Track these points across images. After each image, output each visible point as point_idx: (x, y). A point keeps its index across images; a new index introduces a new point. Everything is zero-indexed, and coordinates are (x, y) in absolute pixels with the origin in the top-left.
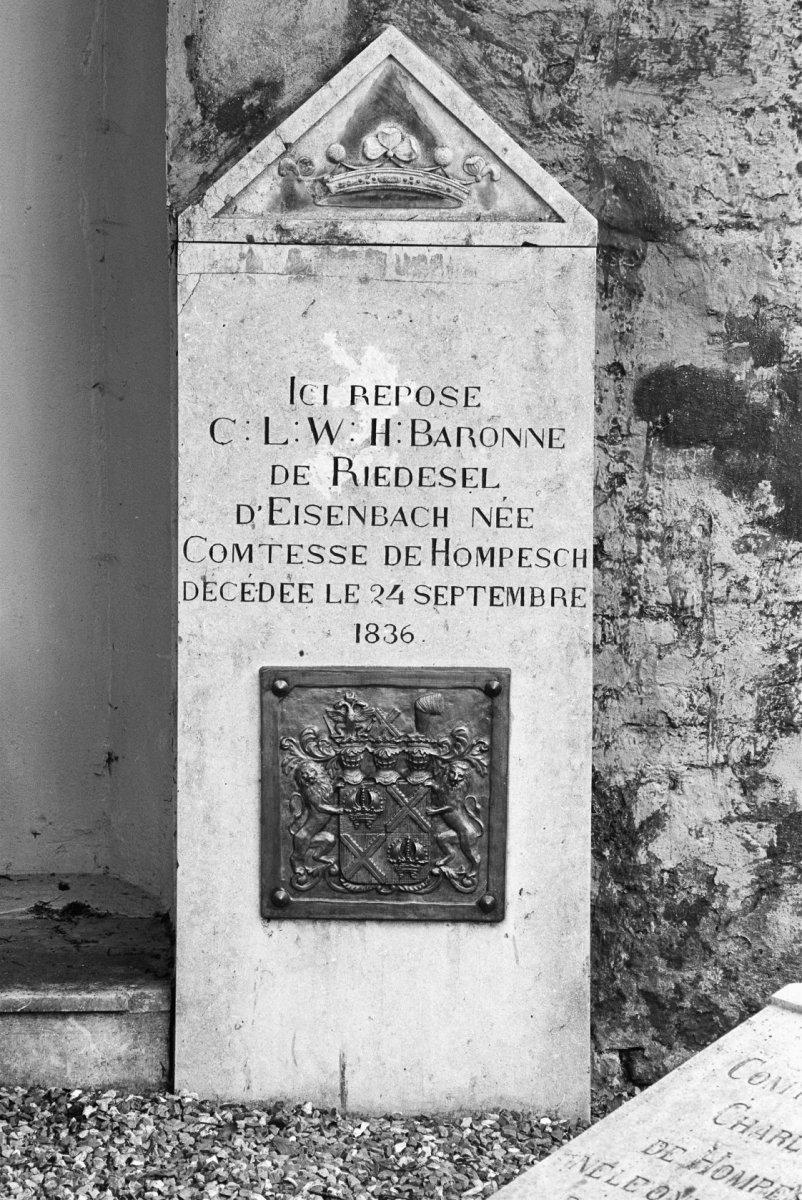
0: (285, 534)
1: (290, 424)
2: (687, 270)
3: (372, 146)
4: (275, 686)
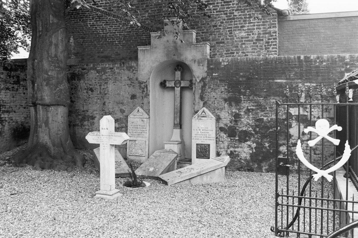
0: (198, 136)
1: (198, 129)
2: (222, 121)
3: (202, 114)
4: (197, 144)
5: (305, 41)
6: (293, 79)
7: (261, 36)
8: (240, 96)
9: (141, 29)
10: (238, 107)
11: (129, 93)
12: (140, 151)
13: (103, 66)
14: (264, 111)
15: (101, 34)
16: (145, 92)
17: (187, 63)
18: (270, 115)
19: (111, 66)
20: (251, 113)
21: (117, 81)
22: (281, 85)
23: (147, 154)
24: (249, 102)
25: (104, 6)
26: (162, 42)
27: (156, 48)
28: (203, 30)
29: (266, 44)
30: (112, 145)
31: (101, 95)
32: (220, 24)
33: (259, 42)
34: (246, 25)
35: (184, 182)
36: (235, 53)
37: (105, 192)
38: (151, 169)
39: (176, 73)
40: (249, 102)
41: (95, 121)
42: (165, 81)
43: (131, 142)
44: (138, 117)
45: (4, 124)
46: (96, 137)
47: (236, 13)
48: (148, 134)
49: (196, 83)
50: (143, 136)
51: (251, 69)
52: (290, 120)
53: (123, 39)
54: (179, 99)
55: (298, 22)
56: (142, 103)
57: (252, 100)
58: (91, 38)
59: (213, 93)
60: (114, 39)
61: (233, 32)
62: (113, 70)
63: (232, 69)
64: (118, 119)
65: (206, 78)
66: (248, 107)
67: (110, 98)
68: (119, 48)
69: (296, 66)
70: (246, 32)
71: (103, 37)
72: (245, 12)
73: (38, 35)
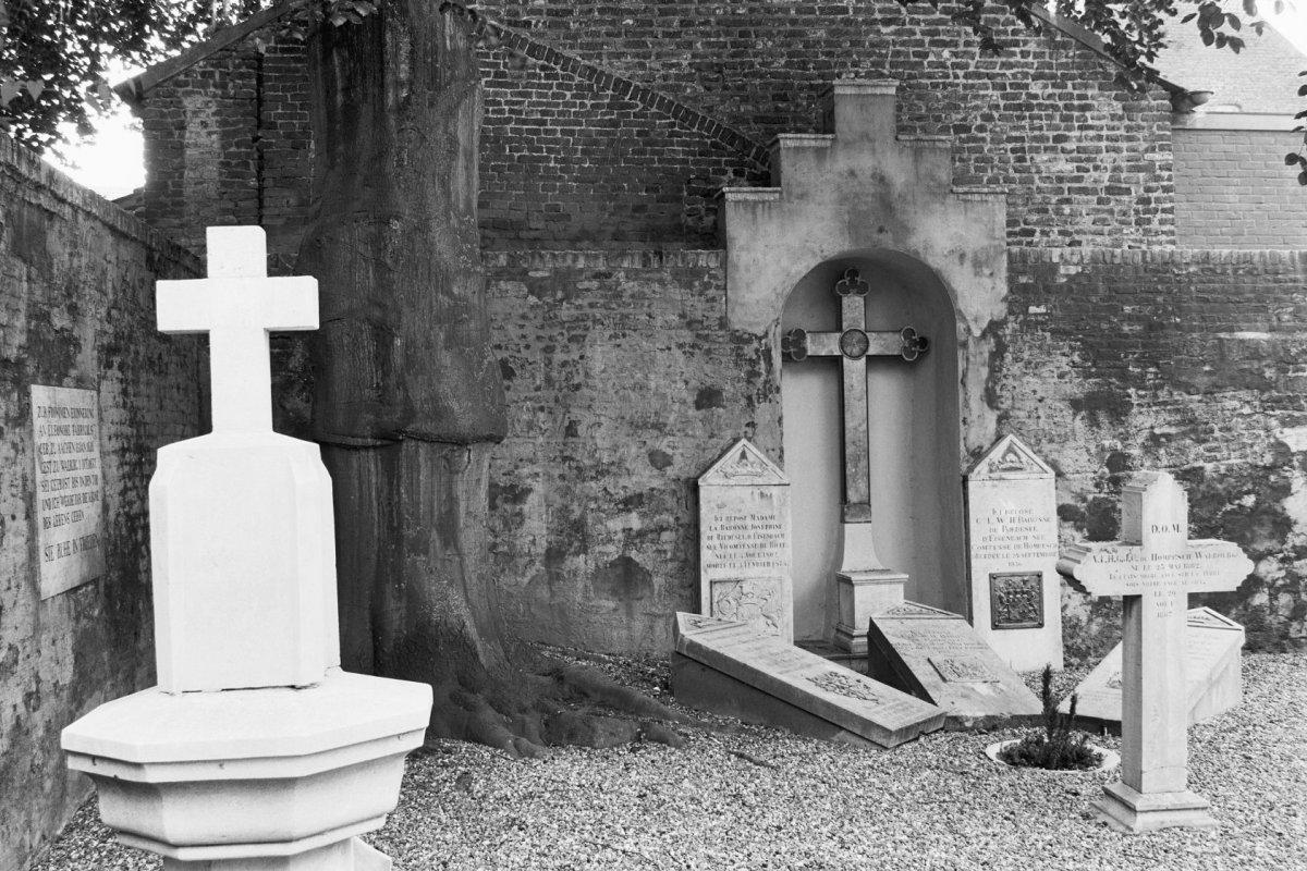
4: (993, 577)
5: (1240, 202)
6: (1291, 331)
7: (1123, 175)
8: (1125, 389)
9: (661, 117)
10: (1121, 430)
11: (686, 383)
13: (559, 264)
14: (1205, 441)
16: (762, 378)
17: (935, 261)
18: (1225, 453)
19: (601, 266)
20: (1162, 451)
21: (627, 332)
22: (1257, 349)
24: (1157, 412)
26: (829, 176)
27: (802, 196)
29: (1141, 207)
30: (1195, 600)
31: (552, 394)
32: (979, 122)
33: (1118, 197)
34: (1072, 134)
36: (1037, 234)
37: (1169, 800)
40: (1154, 409)
41: (526, 508)
42: (800, 335)
46: (1124, 568)
47: (1036, 88)
49: (971, 342)
50: (771, 560)
51: (1159, 293)
52: (1286, 468)
53: (583, 151)
55: (1216, 137)
56: (748, 425)
57: (1165, 403)
61: (1028, 157)
62: (608, 282)
64: (641, 495)
65: (1004, 322)
66: (1152, 427)
67: (596, 404)
68: (565, 190)
69: (1297, 288)
70: (1072, 160)
72: (1066, 87)
73: (390, 100)
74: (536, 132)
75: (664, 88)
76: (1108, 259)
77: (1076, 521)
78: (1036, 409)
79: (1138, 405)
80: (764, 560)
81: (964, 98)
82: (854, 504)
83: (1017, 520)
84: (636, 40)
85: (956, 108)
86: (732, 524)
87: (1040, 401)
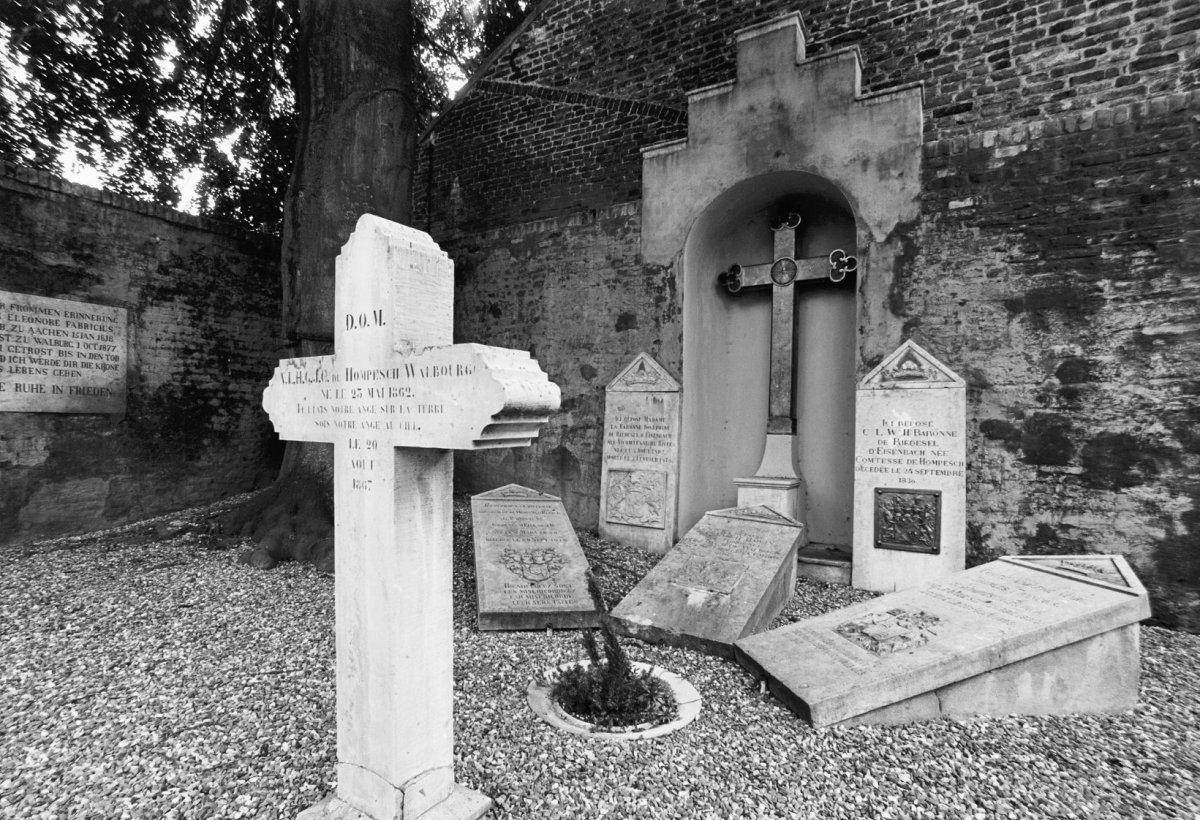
0: (882, 456)
1: (883, 430)
2: (995, 395)
3: (904, 366)
4: (879, 492)
9: (651, 121)
11: (610, 310)
12: (645, 510)
13: (529, 232)
15: (533, 156)
16: (668, 301)
17: (831, 174)
19: (555, 228)
20: (1157, 357)
23: (671, 520)
24: (1148, 306)
25: (542, 76)
27: (705, 141)
28: (881, 78)
31: (523, 325)
32: (950, 41)
35: (903, 707)
38: (698, 597)
39: (778, 235)
40: (1144, 303)
42: (735, 269)
43: (614, 476)
44: (640, 387)
45: (238, 411)
48: (674, 449)
54: (791, 324)
56: (655, 342)
57: (1166, 295)
58: (506, 174)
59: (951, 282)
60: (570, 165)
63: (1048, 170)
64: (573, 400)
65: (917, 223)
71: (538, 165)
74: (568, 153)
75: (653, 99)
76: (1070, 128)
77: (1007, 440)
78: (956, 313)
79: (1114, 300)
80: (653, 456)
81: (933, 23)
82: (777, 417)
83: (912, 433)
84: (636, 70)
85: (923, 36)
86: (629, 423)
87: (961, 304)
